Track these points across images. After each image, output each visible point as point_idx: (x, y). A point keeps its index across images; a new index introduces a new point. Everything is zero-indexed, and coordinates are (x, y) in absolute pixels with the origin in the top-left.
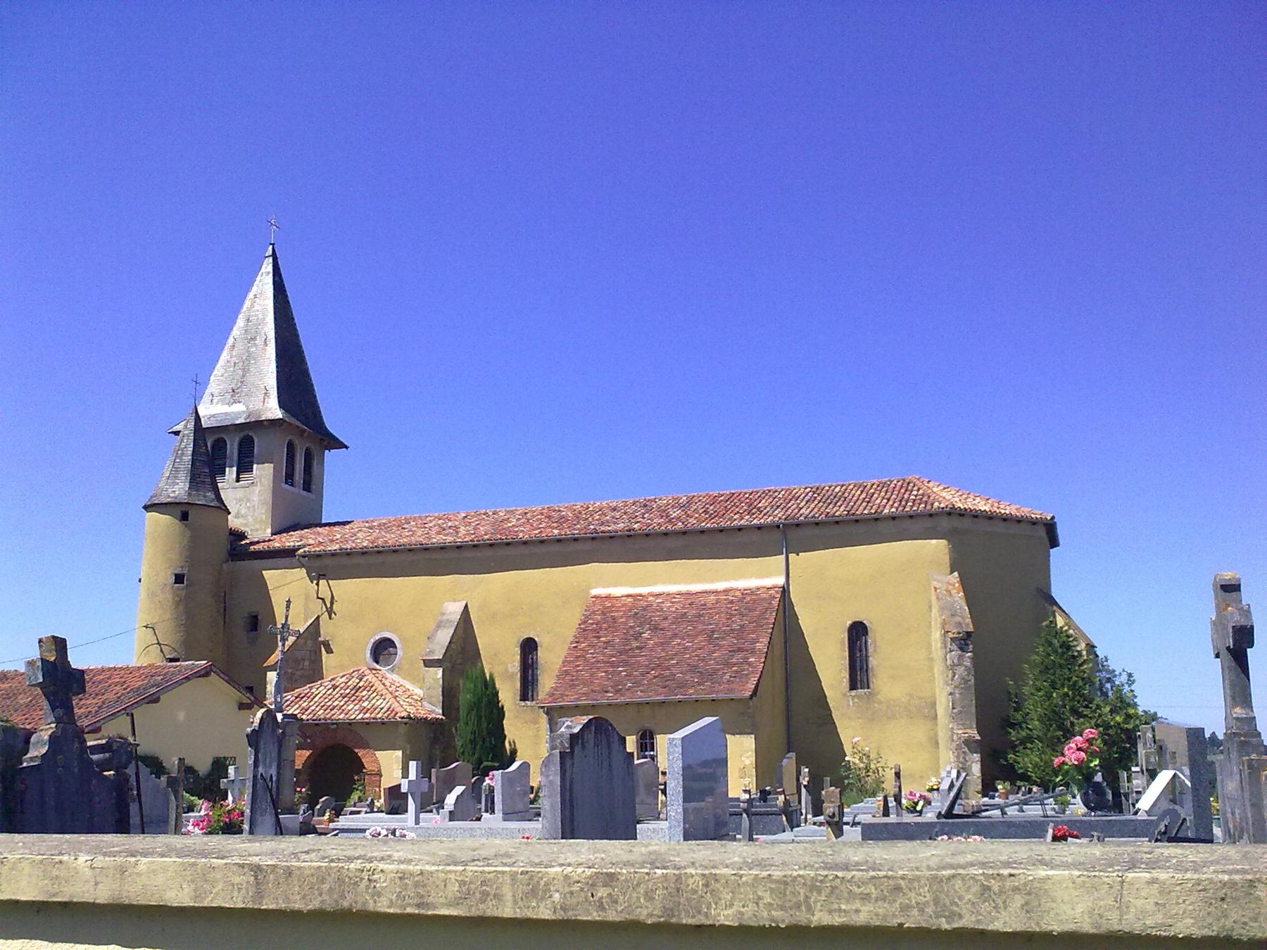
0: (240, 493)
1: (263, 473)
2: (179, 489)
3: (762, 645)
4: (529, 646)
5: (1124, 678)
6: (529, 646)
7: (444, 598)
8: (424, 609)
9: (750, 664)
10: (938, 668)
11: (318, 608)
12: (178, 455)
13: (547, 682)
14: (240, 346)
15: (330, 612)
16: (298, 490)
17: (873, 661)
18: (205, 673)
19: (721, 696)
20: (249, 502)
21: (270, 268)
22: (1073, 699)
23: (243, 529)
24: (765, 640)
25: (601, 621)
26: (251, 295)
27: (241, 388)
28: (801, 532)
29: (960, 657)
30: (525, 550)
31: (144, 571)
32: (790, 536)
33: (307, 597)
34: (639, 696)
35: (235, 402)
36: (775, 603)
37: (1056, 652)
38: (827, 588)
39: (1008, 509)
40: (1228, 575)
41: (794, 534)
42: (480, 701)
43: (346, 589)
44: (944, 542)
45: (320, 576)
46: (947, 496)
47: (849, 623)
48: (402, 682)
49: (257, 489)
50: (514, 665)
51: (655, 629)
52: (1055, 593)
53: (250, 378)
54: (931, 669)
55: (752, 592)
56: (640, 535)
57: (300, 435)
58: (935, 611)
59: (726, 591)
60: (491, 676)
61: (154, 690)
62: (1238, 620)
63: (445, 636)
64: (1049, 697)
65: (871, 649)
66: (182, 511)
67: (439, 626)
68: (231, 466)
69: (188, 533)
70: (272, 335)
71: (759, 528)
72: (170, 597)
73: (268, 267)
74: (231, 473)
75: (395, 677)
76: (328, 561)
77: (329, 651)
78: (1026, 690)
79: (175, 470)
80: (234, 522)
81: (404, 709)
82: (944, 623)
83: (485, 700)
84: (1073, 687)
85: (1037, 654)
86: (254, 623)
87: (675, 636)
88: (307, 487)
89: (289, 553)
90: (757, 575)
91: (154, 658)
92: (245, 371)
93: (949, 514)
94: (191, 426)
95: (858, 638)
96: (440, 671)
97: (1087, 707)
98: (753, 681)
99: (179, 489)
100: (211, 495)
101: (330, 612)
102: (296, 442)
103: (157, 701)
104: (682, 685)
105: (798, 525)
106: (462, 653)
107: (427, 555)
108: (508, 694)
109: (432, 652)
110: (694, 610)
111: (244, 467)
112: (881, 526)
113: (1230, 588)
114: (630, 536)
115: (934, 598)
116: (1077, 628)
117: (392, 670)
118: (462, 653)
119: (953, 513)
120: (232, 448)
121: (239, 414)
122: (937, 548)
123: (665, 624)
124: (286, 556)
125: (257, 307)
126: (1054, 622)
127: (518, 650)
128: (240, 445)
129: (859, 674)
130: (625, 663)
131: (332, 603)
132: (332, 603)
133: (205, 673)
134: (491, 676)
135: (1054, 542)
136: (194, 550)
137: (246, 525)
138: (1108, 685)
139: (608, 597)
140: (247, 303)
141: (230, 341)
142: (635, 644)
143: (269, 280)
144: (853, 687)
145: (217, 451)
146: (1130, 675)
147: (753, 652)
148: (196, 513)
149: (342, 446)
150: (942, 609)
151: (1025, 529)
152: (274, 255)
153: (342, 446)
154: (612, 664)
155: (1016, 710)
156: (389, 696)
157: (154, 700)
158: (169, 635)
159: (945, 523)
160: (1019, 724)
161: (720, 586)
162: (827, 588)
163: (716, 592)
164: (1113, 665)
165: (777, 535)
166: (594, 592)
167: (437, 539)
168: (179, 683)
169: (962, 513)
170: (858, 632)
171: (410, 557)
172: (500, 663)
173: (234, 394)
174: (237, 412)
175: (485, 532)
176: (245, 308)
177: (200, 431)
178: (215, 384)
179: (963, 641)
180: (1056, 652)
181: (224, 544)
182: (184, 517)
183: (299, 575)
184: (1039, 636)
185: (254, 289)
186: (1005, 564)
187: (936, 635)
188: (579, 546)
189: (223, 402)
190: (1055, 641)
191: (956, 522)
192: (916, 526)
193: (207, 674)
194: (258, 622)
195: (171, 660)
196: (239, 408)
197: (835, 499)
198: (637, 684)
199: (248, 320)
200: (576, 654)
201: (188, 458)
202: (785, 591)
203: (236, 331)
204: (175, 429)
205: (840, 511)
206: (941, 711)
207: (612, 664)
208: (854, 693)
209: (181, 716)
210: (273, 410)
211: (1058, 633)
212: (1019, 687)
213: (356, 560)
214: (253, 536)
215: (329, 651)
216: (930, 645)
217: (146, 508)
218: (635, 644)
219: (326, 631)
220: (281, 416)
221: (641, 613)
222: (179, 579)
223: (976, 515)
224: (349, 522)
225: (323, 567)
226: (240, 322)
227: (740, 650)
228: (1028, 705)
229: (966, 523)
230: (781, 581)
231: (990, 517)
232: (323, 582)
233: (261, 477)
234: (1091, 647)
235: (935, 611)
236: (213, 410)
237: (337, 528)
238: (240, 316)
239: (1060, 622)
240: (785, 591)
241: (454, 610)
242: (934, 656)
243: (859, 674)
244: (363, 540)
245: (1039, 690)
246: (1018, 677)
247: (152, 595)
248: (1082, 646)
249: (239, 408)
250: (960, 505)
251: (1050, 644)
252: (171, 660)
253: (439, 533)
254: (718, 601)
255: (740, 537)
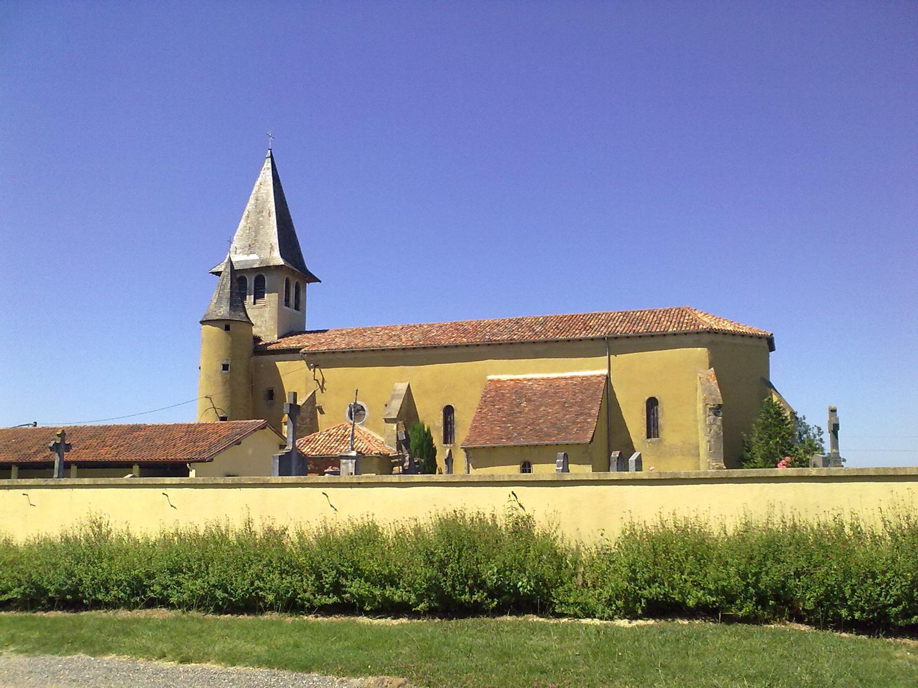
0: (256, 312)
1: (271, 299)
2: (224, 311)
3: (595, 411)
4: (448, 411)
5: (815, 431)
6: (448, 411)
7: (397, 380)
8: (385, 386)
9: (588, 423)
10: (700, 426)
11: (314, 386)
12: (222, 287)
13: (462, 434)
14: (252, 217)
15: (322, 388)
16: (292, 310)
17: (661, 421)
18: (263, 427)
19: (572, 442)
20: (264, 317)
21: (270, 165)
22: (782, 445)
23: (259, 335)
24: (597, 408)
25: (495, 395)
26: (258, 183)
27: (254, 243)
28: (616, 342)
29: (714, 419)
30: (446, 351)
31: (202, 362)
32: (610, 344)
33: (307, 379)
34: (523, 442)
35: (251, 253)
36: (602, 385)
37: (772, 417)
38: (634, 377)
39: (744, 329)
40: (833, 406)
41: (614, 344)
42: (423, 443)
43: (332, 374)
44: (705, 349)
45: (315, 366)
46: (707, 321)
47: (647, 398)
48: (371, 432)
49: (268, 309)
50: (439, 422)
51: (529, 400)
52: (772, 380)
53: (260, 238)
54: (696, 426)
55: (587, 378)
56: (518, 343)
57: (293, 275)
58: (699, 391)
59: (572, 378)
60: (429, 430)
61: (238, 437)
62: (834, 422)
63: (397, 404)
64: (767, 443)
65: (660, 414)
66: (226, 325)
67: (393, 397)
68: (250, 295)
69: (230, 339)
70: (273, 209)
71: (592, 339)
72: (220, 379)
73: (268, 164)
74: (250, 299)
75: (363, 429)
76: (320, 357)
77: (322, 412)
78: (754, 439)
79: (220, 299)
80: (255, 331)
81: (376, 450)
82: (705, 399)
83: (425, 444)
84: (782, 437)
85: (761, 418)
86: (271, 395)
87: (541, 405)
88: (297, 308)
89: (295, 351)
90: (591, 369)
91: (211, 418)
92: (257, 232)
93: (709, 332)
94: (229, 270)
95: (652, 407)
96: (395, 426)
97: (790, 450)
98: (591, 432)
99: (224, 311)
100: (242, 314)
101: (322, 388)
102: (291, 278)
103: (239, 443)
104: (548, 435)
105: (616, 338)
106: (408, 414)
107: (383, 353)
108: (437, 439)
109: (389, 414)
110: (553, 389)
111: (259, 295)
112: (668, 339)
113: (833, 411)
114: (511, 343)
115: (699, 383)
116: (785, 402)
117: (362, 424)
118: (408, 414)
119: (711, 332)
120: (251, 283)
121: (254, 261)
122: (701, 353)
123: (534, 398)
124: (292, 353)
125: (262, 191)
126: (771, 399)
127: (442, 413)
128: (256, 281)
129: (652, 429)
130: (512, 422)
131: (323, 383)
132: (323, 383)
133: (263, 427)
134: (429, 430)
135: (772, 348)
136: (233, 349)
137: (261, 332)
138: (805, 436)
139: (499, 381)
140: (256, 188)
141: (246, 213)
142: (517, 410)
143: (269, 173)
144: (649, 437)
145: (245, 283)
146: (819, 429)
147: (590, 415)
148: (233, 325)
149: (316, 280)
150: (704, 391)
151: (756, 342)
152: (272, 156)
153: (316, 280)
154: (504, 422)
155: (748, 451)
156: (365, 441)
157: (238, 443)
158: (220, 402)
159: (706, 338)
160: (749, 460)
161: (568, 374)
162: (634, 377)
163: (565, 378)
164: (807, 421)
165: (603, 343)
166: (490, 377)
167: (389, 344)
168: (251, 433)
169: (716, 332)
170: (652, 404)
171: (374, 355)
172: (431, 419)
173: (250, 248)
174: (252, 259)
175: (418, 339)
176: (254, 192)
177: (233, 271)
178: (236, 243)
179: (717, 410)
180: (772, 417)
181: (250, 346)
182: (227, 328)
183: (300, 365)
184: (762, 406)
185: (260, 179)
186: (741, 361)
187: (700, 406)
188: (477, 349)
189: (243, 253)
190: (772, 410)
191: (713, 337)
192: (688, 339)
193: (264, 428)
194: (273, 394)
195: (223, 419)
196: (254, 257)
197: (640, 320)
198: (520, 434)
199: (257, 200)
200: (481, 415)
201: (228, 290)
202: (608, 378)
203: (249, 207)
204: (214, 270)
205: (641, 329)
206: (702, 452)
207: (504, 422)
208: (649, 440)
209: (250, 452)
210: (277, 259)
211: (773, 405)
212: (749, 438)
213: (338, 356)
214: (265, 340)
215: (322, 412)
216: (696, 411)
217: (202, 322)
218: (517, 410)
219: (320, 400)
220: (283, 263)
221: (519, 390)
222: (225, 367)
223: (725, 333)
224: (326, 331)
225: (318, 360)
226: (252, 201)
227: (582, 414)
228: (755, 449)
229: (719, 338)
230: (605, 372)
231: (733, 334)
232: (317, 370)
233: (270, 301)
234: (793, 414)
235: (699, 391)
236: (241, 258)
237: (319, 335)
238: (252, 196)
239: (775, 398)
240: (608, 378)
241: (402, 388)
242: (699, 418)
243: (652, 429)
244: (341, 344)
245: (761, 439)
246: (750, 432)
247: (208, 378)
248: (788, 413)
249: (254, 257)
250: (715, 327)
251: (768, 412)
252: (223, 419)
253: (389, 339)
254: (567, 384)
255: (581, 345)
